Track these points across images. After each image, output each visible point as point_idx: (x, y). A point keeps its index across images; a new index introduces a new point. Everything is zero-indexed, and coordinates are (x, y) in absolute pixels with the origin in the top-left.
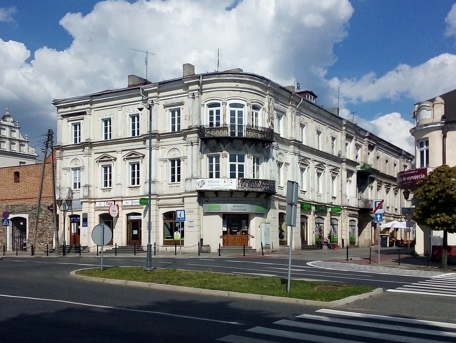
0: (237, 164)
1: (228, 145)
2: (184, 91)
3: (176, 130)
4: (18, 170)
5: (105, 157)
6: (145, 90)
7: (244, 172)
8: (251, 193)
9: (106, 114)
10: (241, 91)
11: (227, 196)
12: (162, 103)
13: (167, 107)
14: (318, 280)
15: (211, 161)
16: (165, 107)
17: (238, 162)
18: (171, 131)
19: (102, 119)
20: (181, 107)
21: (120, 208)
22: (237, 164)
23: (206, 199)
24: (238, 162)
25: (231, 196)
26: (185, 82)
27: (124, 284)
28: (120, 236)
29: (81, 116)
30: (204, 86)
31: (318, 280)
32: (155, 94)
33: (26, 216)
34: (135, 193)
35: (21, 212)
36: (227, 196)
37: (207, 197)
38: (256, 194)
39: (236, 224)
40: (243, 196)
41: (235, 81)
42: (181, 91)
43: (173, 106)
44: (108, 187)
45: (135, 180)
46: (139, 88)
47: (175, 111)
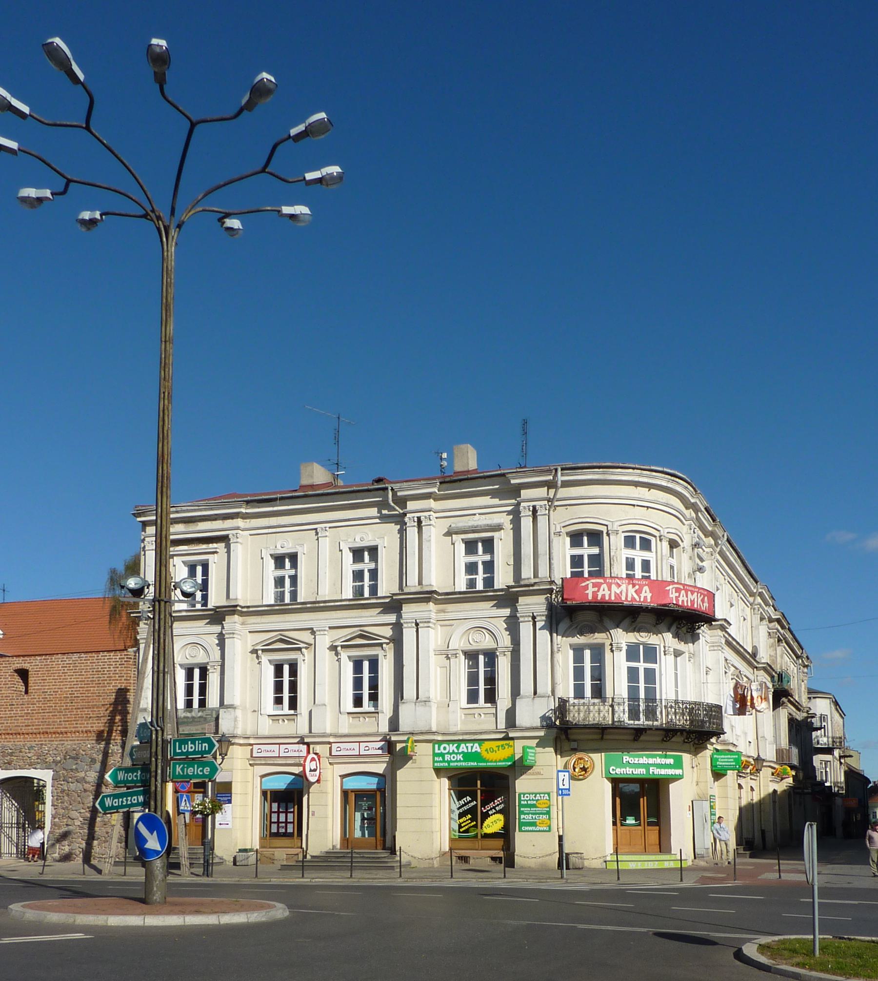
0: (642, 666)
1: (626, 622)
2: (496, 501)
3: (287, 599)
4: (26, 666)
5: (281, 641)
6: (399, 494)
7: (627, 684)
8: (608, 730)
9: (285, 544)
10: (648, 507)
11: (595, 737)
12: (443, 525)
13: (456, 533)
14: (863, 938)
15: (578, 658)
16: (449, 533)
17: (644, 662)
18: (351, 597)
19: (271, 555)
20: (496, 535)
21: (325, 762)
22: (642, 666)
23: (574, 745)
24: (644, 662)
25: (602, 738)
26: (513, 482)
27: (217, 922)
28: (325, 825)
29: (211, 545)
30: (563, 492)
31: (863, 938)
32: (542, 492)
33: (45, 775)
34: (366, 725)
35: (32, 765)
36: (595, 737)
37: (575, 741)
38: (632, 731)
39: (641, 803)
40: (632, 737)
41: (637, 484)
42: (486, 500)
43: (474, 532)
44: (286, 709)
45: (365, 692)
46: (386, 489)
47: (480, 543)
